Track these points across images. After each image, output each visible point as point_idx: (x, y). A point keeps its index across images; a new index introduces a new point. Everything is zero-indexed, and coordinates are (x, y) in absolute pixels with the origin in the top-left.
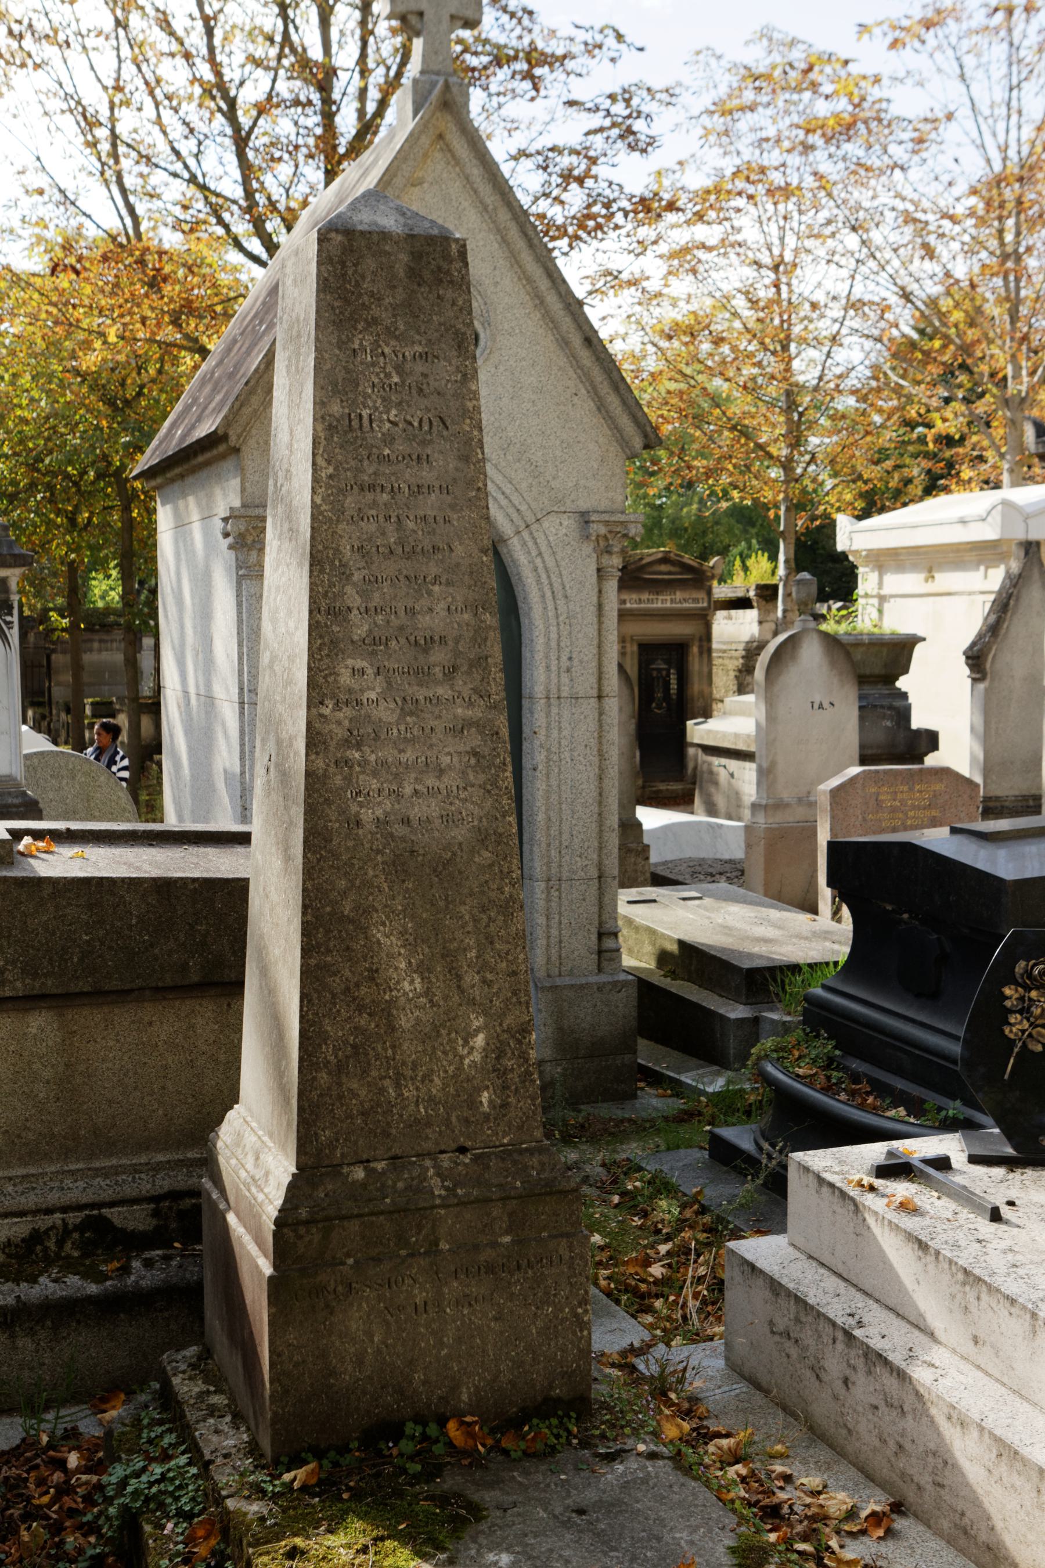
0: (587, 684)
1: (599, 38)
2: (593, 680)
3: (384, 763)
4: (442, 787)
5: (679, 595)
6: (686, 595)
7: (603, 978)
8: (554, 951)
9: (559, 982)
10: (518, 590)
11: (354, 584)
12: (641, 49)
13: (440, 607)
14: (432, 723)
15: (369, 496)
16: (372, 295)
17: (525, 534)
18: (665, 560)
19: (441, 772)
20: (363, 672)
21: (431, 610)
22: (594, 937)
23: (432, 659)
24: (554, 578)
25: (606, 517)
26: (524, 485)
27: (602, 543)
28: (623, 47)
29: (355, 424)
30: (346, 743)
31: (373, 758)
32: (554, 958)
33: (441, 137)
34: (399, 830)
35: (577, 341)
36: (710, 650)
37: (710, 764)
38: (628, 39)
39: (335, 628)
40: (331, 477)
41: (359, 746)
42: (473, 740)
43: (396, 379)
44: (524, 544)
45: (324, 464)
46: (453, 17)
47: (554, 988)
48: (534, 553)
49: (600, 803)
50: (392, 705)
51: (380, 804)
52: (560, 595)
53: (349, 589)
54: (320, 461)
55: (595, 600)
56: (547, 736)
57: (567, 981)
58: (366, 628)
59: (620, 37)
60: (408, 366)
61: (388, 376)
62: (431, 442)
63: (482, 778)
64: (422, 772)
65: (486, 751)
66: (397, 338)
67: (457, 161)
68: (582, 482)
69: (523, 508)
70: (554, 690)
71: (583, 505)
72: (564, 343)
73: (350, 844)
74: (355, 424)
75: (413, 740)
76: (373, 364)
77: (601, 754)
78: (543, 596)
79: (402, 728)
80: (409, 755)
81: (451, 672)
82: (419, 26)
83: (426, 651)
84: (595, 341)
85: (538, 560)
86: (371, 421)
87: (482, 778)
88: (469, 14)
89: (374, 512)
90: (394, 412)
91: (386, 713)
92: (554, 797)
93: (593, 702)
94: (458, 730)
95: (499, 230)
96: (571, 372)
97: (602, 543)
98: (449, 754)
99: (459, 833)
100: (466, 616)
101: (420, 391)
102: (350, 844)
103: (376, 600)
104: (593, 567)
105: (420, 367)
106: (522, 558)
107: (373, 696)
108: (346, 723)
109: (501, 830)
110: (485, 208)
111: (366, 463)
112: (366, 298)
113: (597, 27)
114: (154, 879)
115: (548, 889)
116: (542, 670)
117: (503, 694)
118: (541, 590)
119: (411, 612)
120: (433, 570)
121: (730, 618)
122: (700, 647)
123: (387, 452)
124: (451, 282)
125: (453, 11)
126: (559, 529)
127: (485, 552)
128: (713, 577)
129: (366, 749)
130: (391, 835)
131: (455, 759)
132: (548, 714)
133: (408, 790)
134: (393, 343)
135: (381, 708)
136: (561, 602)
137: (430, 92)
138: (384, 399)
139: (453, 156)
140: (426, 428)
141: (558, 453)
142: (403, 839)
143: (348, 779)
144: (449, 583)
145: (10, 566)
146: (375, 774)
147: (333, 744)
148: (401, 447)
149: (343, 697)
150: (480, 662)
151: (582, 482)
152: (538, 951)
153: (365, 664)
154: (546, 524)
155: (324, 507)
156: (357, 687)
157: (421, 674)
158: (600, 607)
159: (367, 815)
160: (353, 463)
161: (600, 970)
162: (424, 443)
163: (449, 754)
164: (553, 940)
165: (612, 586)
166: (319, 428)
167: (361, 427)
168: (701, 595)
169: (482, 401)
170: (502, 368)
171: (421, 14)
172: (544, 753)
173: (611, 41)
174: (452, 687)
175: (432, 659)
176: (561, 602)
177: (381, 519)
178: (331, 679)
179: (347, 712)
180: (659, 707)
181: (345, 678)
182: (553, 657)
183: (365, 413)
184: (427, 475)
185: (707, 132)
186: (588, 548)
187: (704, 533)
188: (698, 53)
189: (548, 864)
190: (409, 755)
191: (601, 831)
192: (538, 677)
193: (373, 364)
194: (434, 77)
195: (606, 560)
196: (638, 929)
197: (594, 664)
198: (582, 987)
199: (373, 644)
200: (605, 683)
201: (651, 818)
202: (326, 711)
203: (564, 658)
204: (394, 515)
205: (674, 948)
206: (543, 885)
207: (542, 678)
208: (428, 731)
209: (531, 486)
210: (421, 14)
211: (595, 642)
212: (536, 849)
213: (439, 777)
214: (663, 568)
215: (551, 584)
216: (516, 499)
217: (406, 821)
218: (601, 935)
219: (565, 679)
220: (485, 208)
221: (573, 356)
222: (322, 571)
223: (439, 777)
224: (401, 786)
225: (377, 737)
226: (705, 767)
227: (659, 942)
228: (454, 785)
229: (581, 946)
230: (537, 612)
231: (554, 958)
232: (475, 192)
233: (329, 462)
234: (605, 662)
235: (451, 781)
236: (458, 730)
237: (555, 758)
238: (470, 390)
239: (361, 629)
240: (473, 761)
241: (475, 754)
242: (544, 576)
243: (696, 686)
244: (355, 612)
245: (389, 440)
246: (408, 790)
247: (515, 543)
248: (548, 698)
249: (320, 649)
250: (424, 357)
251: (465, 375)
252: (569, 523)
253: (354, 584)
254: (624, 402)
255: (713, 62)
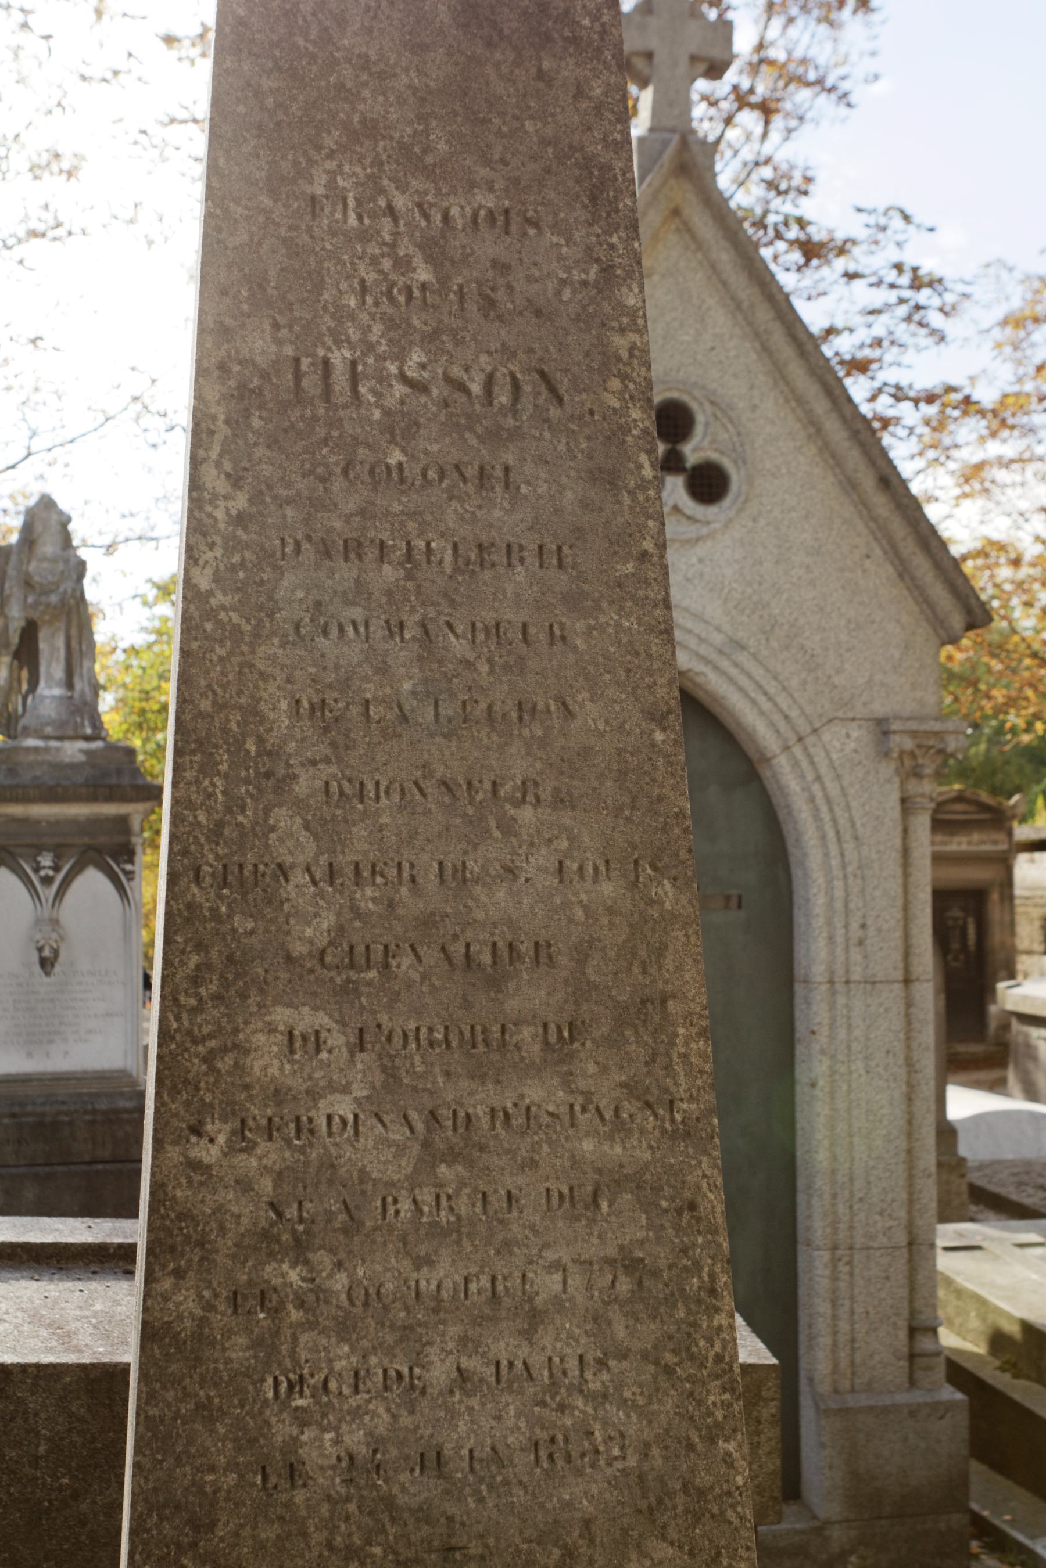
0: (887, 961)
1: (882, 221)
2: (897, 956)
3: (372, 1298)
4: (537, 1360)
5: (976, 837)
6: (984, 836)
7: (917, 1397)
8: (843, 1355)
9: (851, 1401)
10: (787, 829)
11: (300, 805)
12: (931, 230)
13: (537, 865)
14: (510, 1182)
15: (345, 573)
16: (365, 64)
17: (797, 751)
18: (960, 798)
19: (533, 1319)
20: (317, 1041)
21: (511, 871)
22: (903, 1335)
23: (512, 1005)
24: (838, 812)
25: (913, 726)
26: (794, 683)
27: (908, 763)
28: (911, 228)
29: (311, 384)
30: (265, 1243)
31: (340, 1282)
32: (844, 1364)
33: (676, 212)
34: (412, 1488)
35: (868, 481)
36: (1011, 898)
37: (1027, 1036)
38: (916, 219)
39: (242, 923)
40: (240, 519)
41: (300, 1250)
42: (626, 1226)
43: (424, 274)
44: (796, 764)
45: (222, 486)
46: (694, 59)
47: (845, 1412)
48: (810, 776)
49: (909, 1135)
50: (398, 1134)
51: (356, 1413)
52: (847, 836)
53: (282, 817)
54: (214, 481)
55: (898, 842)
56: (832, 1037)
57: (865, 1400)
58: (328, 920)
59: (907, 218)
60: (456, 243)
61: (403, 264)
62: (515, 434)
63: (650, 1331)
64: (479, 1321)
65: (663, 1256)
66: (428, 172)
67: (699, 245)
68: (878, 677)
69: (794, 713)
70: (840, 972)
71: (880, 708)
72: (850, 486)
73: (269, 1533)
74: (311, 384)
75: (456, 1231)
76: (364, 236)
77: (909, 1063)
78: (823, 838)
79: (426, 1196)
80: (443, 1273)
81: (563, 1042)
82: (646, 71)
83: (495, 982)
84: (894, 480)
85: (816, 788)
86: (354, 379)
87: (650, 1331)
88: (716, 53)
89: (357, 613)
90: (417, 356)
91: (380, 1155)
92: (841, 1127)
93: (898, 988)
94: (581, 1201)
95: (757, 335)
96: (860, 526)
97: (908, 763)
98: (557, 1266)
99: (585, 1493)
100: (607, 889)
101: (489, 304)
102: (269, 1533)
103: (360, 843)
104: (895, 796)
105: (489, 246)
106: (793, 785)
107: (344, 1107)
108: (267, 1185)
109: (703, 1479)
110: (739, 306)
111: (338, 485)
112: (347, 72)
113: (881, 209)
114: (83, 1368)
115: (835, 1261)
116: (822, 943)
117: (709, 1098)
118: (820, 828)
119: (457, 878)
120: (518, 766)
121: (1032, 861)
122: (1001, 894)
123: (396, 457)
124: (575, 40)
125: (693, 49)
126: (845, 742)
127: (660, 719)
128: (1013, 817)
129: (323, 1259)
130: (389, 1503)
131: (576, 1282)
132: (832, 1006)
133: (439, 1372)
134: (417, 183)
135: (366, 1141)
136: (849, 846)
137: (661, 153)
138: (390, 324)
139: (694, 237)
140: (503, 398)
141: (843, 637)
142: (423, 1514)
143: (266, 1345)
144: (559, 801)
145: (131, 800)
146: (345, 1329)
147: (226, 1244)
148: (433, 445)
149: (258, 1112)
150: (648, 1009)
151: (878, 677)
152: (821, 1355)
153: (323, 1020)
154: (826, 737)
155: (219, 599)
156: (298, 1084)
157: (484, 1049)
158: (906, 852)
159: (319, 1448)
160: (302, 485)
161: (912, 1382)
162: (495, 437)
163: (557, 1266)
164: (842, 1338)
165: (922, 823)
166: (212, 394)
167: (327, 392)
168: (1001, 836)
169: (656, 332)
170: (762, 522)
171: (649, 56)
172: (826, 1062)
173: (897, 222)
174: (567, 1081)
175: (512, 1005)
176: (849, 846)
177: (378, 632)
178: (225, 1064)
179: (270, 1153)
180: (956, 959)
181: (267, 1062)
182: (839, 922)
183: (340, 357)
184: (504, 520)
185: (999, 345)
186: (887, 769)
187: (994, 773)
188: (988, 265)
189: (834, 1225)
190: (443, 1273)
191: (911, 1177)
192: (817, 951)
193: (364, 236)
194: (667, 135)
195: (914, 787)
196: (960, 1292)
197: (898, 933)
198: (886, 1410)
199: (348, 967)
200: (914, 961)
201: (964, 1103)
202: (209, 1153)
203: (855, 925)
204: (412, 621)
205: (1013, 1330)
206: (826, 1256)
207: (823, 954)
208: (497, 1202)
209: (804, 683)
210: (649, 56)
211: (900, 903)
212: (815, 1201)
213: (528, 1334)
214: (959, 807)
215: (834, 820)
216: (783, 701)
217: (433, 1462)
218: (913, 1331)
219: (856, 955)
220: (739, 306)
221: (864, 504)
222: (209, 768)
223: (528, 1334)
224: (419, 1361)
225: (353, 1225)
226: (1020, 1039)
227: (991, 1318)
228: (572, 1353)
229: (884, 1346)
230: (814, 859)
231: (844, 1364)
232: (724, 284)
233: (236, 481)
234: (914, 931)
235: (562, 1343)
236: (581, 1201)
237: (843, 1069)
238: (621, 308)
239: (313, 929)
240: (624, 1285)
241: (632, 1265)
242: (824, 809)
243: (996, 936)
244: (300, 877)
245: (401, 427)
246: (439, 1372)
247: (782, 763)
248: (831, 982)
249: (196, 981)
250: (500, 220)
251: (607, 270)
252: (859, 735)
253: (300, 805)
254: (937, 565)
255: (1004, 274)
